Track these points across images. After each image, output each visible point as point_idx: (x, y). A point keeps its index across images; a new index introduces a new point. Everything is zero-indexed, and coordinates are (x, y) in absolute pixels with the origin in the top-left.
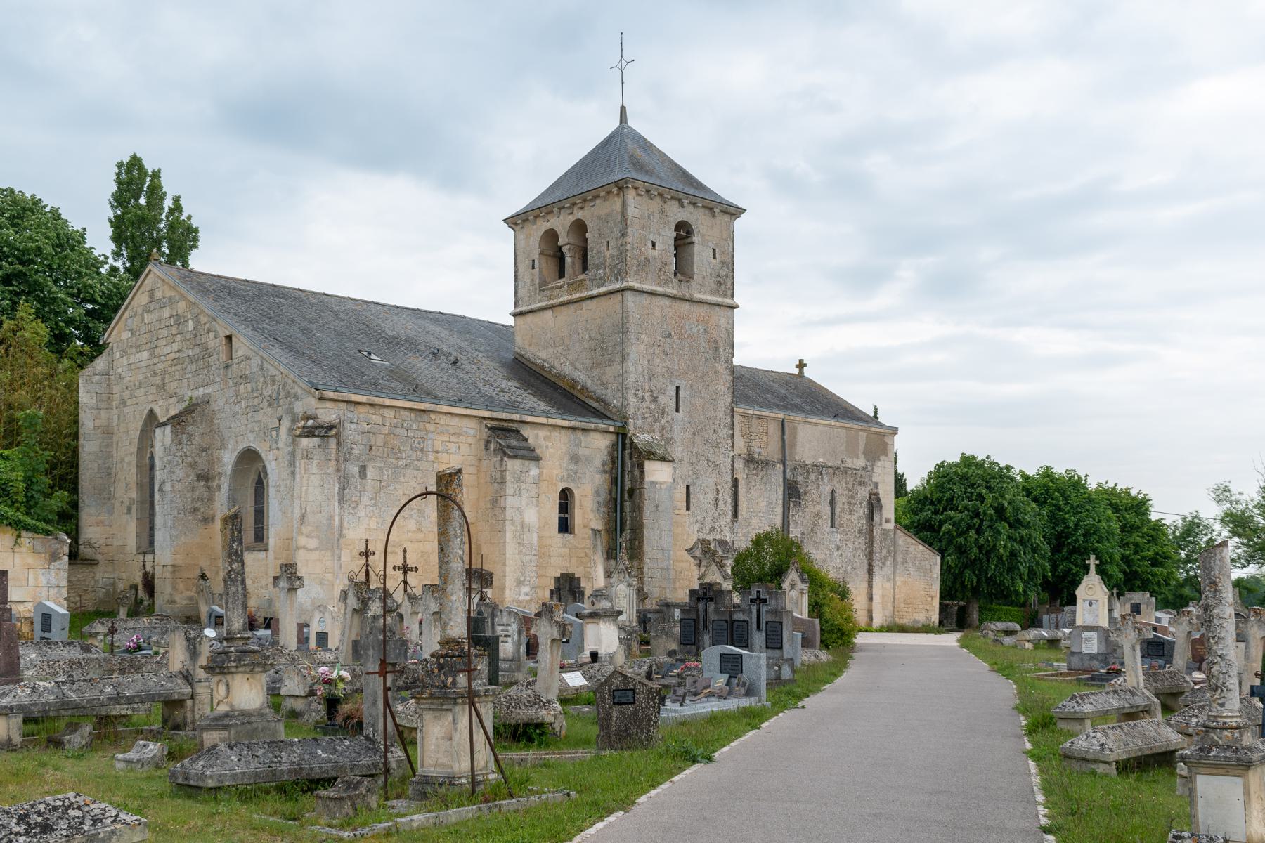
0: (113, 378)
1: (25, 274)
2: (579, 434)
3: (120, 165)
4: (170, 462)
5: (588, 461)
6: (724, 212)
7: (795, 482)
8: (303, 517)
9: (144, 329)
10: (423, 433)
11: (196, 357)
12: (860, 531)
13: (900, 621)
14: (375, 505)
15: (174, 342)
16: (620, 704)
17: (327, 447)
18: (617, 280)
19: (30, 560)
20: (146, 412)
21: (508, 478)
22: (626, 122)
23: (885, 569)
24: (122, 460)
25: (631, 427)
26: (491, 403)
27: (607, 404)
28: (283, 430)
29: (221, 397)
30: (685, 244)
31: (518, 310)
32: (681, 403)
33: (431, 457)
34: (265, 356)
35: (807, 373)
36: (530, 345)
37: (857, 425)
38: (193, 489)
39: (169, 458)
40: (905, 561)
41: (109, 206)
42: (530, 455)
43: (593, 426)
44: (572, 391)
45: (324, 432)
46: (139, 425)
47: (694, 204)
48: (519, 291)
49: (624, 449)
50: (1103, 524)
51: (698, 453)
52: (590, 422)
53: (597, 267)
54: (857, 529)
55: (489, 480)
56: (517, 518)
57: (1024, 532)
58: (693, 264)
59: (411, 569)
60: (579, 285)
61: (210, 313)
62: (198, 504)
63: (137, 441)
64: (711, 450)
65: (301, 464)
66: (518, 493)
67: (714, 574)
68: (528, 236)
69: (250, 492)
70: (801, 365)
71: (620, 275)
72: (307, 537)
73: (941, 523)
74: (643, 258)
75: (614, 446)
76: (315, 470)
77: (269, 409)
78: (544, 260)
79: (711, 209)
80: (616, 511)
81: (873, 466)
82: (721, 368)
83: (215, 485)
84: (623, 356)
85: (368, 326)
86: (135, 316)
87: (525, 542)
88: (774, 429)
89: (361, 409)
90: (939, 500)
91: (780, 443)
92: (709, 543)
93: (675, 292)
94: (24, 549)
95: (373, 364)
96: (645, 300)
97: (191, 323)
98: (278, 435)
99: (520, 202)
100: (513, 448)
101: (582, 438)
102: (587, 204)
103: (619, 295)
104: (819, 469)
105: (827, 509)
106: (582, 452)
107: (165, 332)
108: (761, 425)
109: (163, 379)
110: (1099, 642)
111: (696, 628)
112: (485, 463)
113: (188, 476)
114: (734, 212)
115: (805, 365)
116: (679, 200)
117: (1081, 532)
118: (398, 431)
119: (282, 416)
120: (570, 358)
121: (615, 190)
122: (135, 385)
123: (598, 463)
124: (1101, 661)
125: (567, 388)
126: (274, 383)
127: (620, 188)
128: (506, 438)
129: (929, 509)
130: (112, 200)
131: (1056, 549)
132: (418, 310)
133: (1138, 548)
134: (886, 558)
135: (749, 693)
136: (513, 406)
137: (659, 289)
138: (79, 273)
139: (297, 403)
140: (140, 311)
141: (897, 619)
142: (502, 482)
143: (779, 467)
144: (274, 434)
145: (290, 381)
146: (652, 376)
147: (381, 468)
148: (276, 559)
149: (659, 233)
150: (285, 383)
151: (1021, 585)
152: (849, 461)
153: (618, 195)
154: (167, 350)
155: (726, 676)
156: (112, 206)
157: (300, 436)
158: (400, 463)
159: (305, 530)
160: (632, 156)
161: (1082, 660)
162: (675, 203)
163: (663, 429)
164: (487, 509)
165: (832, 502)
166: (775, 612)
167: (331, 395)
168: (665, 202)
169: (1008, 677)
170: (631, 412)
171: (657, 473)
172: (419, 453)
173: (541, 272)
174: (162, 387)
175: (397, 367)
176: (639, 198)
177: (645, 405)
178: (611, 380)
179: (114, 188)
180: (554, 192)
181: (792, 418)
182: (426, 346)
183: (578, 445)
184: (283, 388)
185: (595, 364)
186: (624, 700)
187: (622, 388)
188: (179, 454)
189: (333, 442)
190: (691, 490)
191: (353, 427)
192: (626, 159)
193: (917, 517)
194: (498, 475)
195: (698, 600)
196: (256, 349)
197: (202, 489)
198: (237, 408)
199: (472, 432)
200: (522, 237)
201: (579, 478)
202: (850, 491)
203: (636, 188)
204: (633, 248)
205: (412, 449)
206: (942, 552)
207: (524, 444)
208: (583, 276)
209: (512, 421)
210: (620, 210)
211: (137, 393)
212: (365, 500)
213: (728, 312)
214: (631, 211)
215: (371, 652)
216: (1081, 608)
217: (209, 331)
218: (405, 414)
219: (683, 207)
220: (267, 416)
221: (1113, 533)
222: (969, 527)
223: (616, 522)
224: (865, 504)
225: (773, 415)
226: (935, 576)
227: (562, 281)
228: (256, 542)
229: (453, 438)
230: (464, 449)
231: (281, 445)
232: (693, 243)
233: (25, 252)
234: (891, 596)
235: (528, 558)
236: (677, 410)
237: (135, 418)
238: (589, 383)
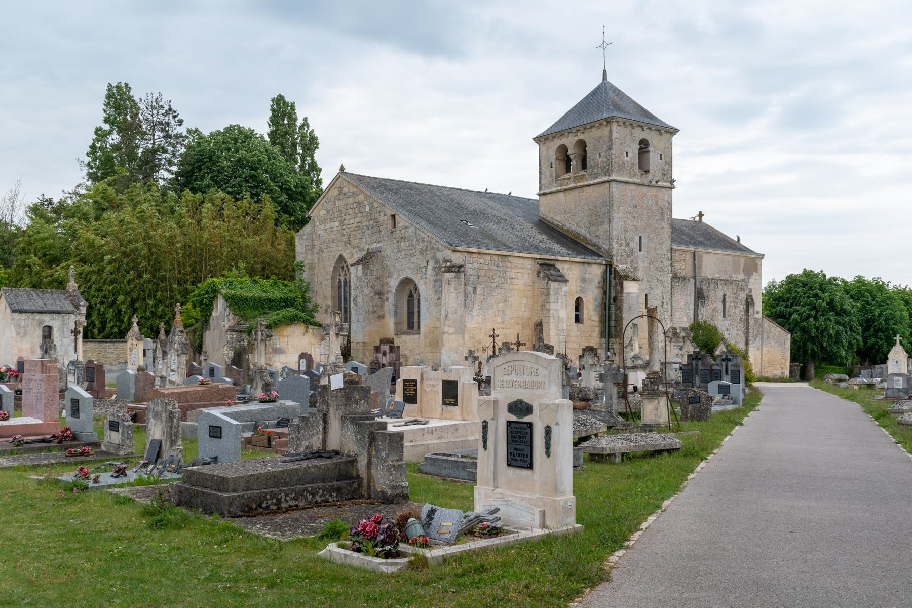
0: (314, 236)
1: (256, 176)
2: (586, 266)
3: (273, 100)
4: (361, 286)
5: (590, 281)
7: (702, 289)
8: (447, 316)
9: (335, 209)
10: (504, 268)
11: (371, 226)
12: (741, 319)
13: (764, 375)
14: (481, 308)
15: (356, 217)
16: (692, 403)
17: (459, 278)
18: (606, 175)
19: (312, 340)
20: (337, 256)
21: (551, 293)
22: (607, 79)
23: (756, 342)
24: (321, 283)
25: (615, 261)
26: (537, 249)
27: (599, 248)
28: (430, 268)
29: (388, 249)
30: (643, 152)
31: (542, 192)
32: (642, 246)
33: (509, 281)
34: (418, 227)
35: (705, 220)
36: (550, 213)
37: (739, 254)
39: (361, 283)
40: (768, 338)
41: (268, 125)
42: (562, 279)
43: (594, 261)
44: (577, 240)
45: (458, 269)
46: (333, 263)
47: (650, 129)
48: (542, 181)
49: (610, 274)
50: (898, 313)
51: (652, 275)
52: (592, 259)
53: (593, 167)
54: (739, 318)
55: (539, 294)
56: (556, 315)
57: (846, 319)
58: (649, 164)
59: (522, 344)
60: (582, 178)
61: (381, 202)
63: (331, 272)
64: (659, 273)
65: (445, 287)
66: (556, 301)
67: (688, 346)
68: (548, 148)
69: (405, 301)
70: (701, 215)
71: (608, 172)
72: (449, 327)
73: (790, 314)
74: (621, 162)
75: (605, 272)
76: (452, 290)
77: (420, 256)
78: (558, 162)
79: (659, 131)
80: (606, 310)
81: (748, 279)
82: (665, 224)
83: (384, 298)
85: (458, 204)
86: (329, 202)
87: (561, 328)
88: (689, 258)
89: (474, 256)
90: (788, 299)
91: (693, 266)
92: (676, 329)
93: (639, 181)
94: (309, 335)
95: (471, 228)
96: (622, 186)
97: (367, 207)
98: (426, 270)
100: (553, 275)
101: (588, 268)
102: (587, 130)
103: (607, 185)
104: (716, 281)
105: (721, 306)
106: (588, 276)
107: (350, 212)
108: (681, 255)
109: (349, 238)
110: (904, 382)
111: (692, 374)
112: (537, 284)
113: (370, 293)
114: (673, 131)
115: (703, 215)
116: (642, 127)
117: (883, 318)
118: (492, 267)
119: (428, 260)
120: (576, 220)
121: (605, 123)
122: (329, 241)
123: (596, 282)
124: (905, 393)
125: (574, 238)
126: (423, 241)
127: (608, 122)
128: (549, 270)
129: (782, 305)
130: (269, 122)
131: (866, 330)
132: (479, 192)
134: (757, 336)
135: (734, 403)
136: (548, 251)
137: (630, 180)
138: (281, 174)
139: (439, 253)
140: (333, 199)
141: (763, 374)
142: (548, 295)
143: (692, 281)
144: (424, 270)
145: (434, 241)
146: (626, 231)
147: (484, 288)
148: (425, 339)
149: (630, 147)
150: (431, 242)
151: (844, 352)
152: (734, 276)
153: (606, 126)
154: (352, 221)
155: (722, 395)
156: (269, 125)
157: (445, 272)
158: (493, 285)
159: (448, 323)
160: (613, 101)
161: (893, 392)
162: (639, 129)
163: (632, 262)
164: (538, 310)
165: (724, 302)
166: (735, 365)
167: (460, 249)
168: (634, 129)
169: (852, 400)
170: (614, 252)
171: (630, 287)
172: (503, 280)
173: (556, 170)
174: (348, 242)
175: (483, 229)
176: (619, 127)
177: (622, 248)
178: (602, 233)
179: (270, 114)
180: (564, 122)
181: (700, 250)
182: (492, 215)
183: (585, 272)
184: (430, 244)
185: (592, 224)
186: (694, 402)
187: (609, 238)
188: (366, 281)
189: (462, 274)
190: (648, 297)
191: (470, 266)
192: (610, 103)
193: (775, 310)
194: (545, 291)
195: (693, 359)
196: (412, 223)
197: (378, 300)
198: (399, 255)
199: (529, 266)
200: (544, 149)
201: (586, 291)
202: (735, 294)
203: (617, 122)
204: (616, 157)
205: (499, 277)
206: (791, 331)
207: (558, 273)
208: (582, 173)
209: (551, 260)
210: (608, 135)
211: (331, 245)
212: (476, 306)
215: (609, 378)
216: (890, 363)
217: (380, 212)
219: (643, 130)
220: (419, 260)
221: (904, 319)
223: (606, 316)
224: (744, 302)
225: (689, 249)
226: (787, 347)
227: (569, 175)
228: (408, 329)
229: (520, 270)
230: (526, 276)
231: (428, 276)
232: (649, 151)
233: (254, 162)
234: (760, 359)
235: (561, 337)
236: (640, 251)
237: (329, 259)
238: (588, 236)
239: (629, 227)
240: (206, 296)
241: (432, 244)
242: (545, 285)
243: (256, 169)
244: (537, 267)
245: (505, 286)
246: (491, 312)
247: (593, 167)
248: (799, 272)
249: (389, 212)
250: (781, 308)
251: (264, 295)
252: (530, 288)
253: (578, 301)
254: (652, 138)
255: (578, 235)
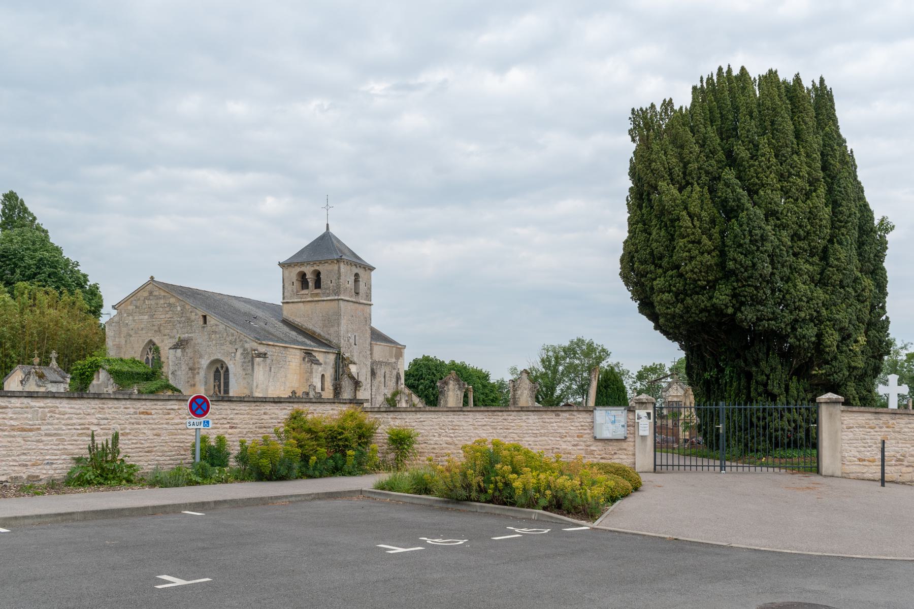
6: (369, 269)
8: (257, 386)
28: (239, 353)
38: (188, 374)
42: (317, 363)
45: (264, 355)
47: (360, 267)
53: (326, 289)
60: (317, 295)
62: (189, 380)
65: (256, 366)
66: (316, 377)
76: (261, 369)
79: (365, 268)
82: (367, 328)
84: (338, 324)
89: (270, 347)
90: (417, 375)
98: (235, 355)
99: (284, 258)
103: (337, 301)
104: (380, 363)
109: (159, 328)
121: (336, 262)
123: (332, 365)
133: (487, 395)
137: (350, 299)
140: (142, 298)
144: (233, 355)
154: (163, 316)
167: (264, 342)
170: (341, 345)
185: (325, 326)
187: (338, 336)
194: (309, 370)
211: (140, 332)
213: (368, 307)
214: (342, 270)
217: (191, 312)
218: (281, 348)
220: (230, 348)
222: (430, 387)
229: (294, 357)
231: (236, 359)
233: (53, 263)
238: (322, 333)
239: (349, 329)
240: (89, 370)
241: (241, 338)
242: (309, 367)
243: (55, 267)
244: (303, 355)
245: (286, 366)
246: (278, 383)
247: (326, 289)
248: (421, 357)
249: (200, 313)
250: (411, 381)
251: (130, 369)
252: (298, 368)
253: (323, 376)
254: (360, 271)
255: (314, 333)
